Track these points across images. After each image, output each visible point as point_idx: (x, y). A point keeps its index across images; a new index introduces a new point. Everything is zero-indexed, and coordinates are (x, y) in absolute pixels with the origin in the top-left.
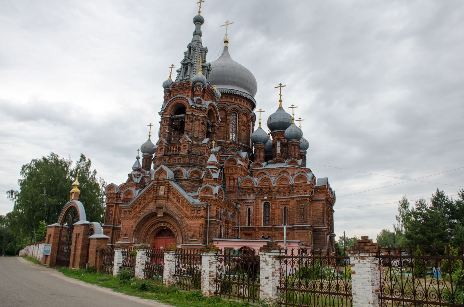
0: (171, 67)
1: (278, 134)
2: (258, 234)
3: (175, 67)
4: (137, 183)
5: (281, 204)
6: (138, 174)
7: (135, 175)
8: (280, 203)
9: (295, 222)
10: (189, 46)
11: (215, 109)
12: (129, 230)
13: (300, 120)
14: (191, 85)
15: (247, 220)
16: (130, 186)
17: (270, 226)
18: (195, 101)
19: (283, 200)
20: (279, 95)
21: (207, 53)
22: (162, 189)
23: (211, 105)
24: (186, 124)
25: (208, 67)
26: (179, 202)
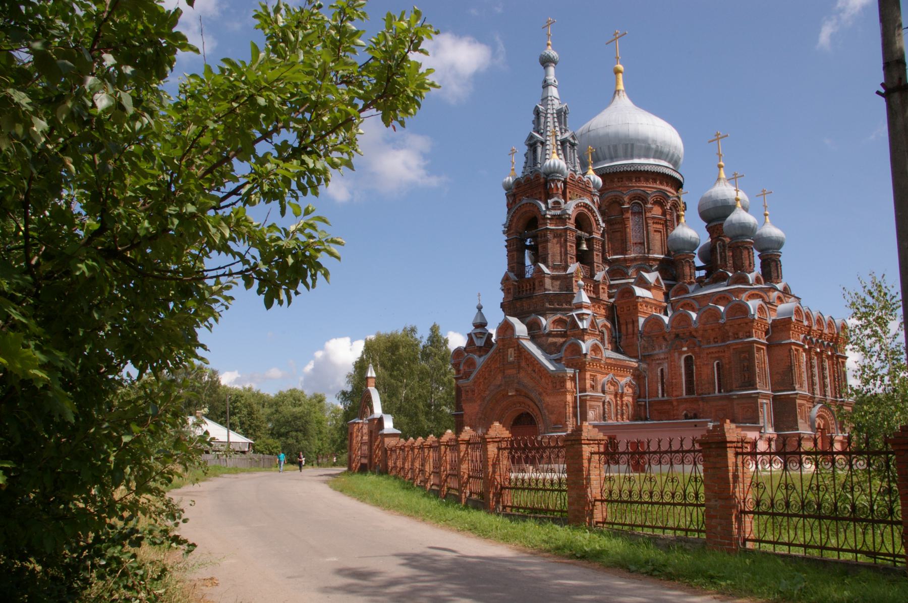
2: (677, 410)
5: (711, 358)
8: (710, 356)
9: (734, 386)
11: (591, 211)
12: (473, 417)
13: (764, 194)
14: (542, 180)
16: (471, 352)
17: (695, 396)
18: (550, 207)
19: (714, 350)
23: (581, 206)
24: (539, 246)
26: (534, 371)
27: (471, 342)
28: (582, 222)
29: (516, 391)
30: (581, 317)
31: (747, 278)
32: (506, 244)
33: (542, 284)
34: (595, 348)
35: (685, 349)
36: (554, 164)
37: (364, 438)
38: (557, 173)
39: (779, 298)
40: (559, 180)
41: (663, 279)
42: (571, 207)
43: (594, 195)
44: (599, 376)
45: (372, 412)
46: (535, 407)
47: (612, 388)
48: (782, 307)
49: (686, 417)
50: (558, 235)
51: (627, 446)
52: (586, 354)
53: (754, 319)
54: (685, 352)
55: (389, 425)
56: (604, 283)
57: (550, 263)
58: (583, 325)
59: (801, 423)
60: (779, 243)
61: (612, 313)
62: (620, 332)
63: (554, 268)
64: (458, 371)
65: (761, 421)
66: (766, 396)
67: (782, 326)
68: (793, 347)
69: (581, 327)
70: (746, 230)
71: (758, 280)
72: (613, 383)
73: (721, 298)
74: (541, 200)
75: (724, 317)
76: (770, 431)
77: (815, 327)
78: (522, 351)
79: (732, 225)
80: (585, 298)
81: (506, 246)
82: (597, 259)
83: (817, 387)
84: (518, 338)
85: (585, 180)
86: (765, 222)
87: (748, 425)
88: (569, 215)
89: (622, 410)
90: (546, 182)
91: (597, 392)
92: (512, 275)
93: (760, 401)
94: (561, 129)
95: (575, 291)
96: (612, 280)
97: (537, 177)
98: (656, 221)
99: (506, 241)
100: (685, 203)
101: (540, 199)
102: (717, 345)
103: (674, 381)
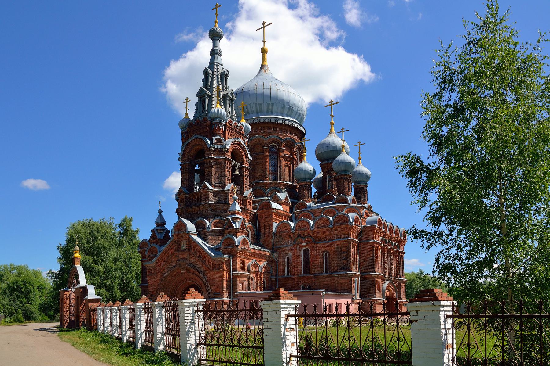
0: (186, 101)
1: (328, 167)
3: (190, 101)
4: (161, 239)
6: (161, 229)
7: (159, 230)
9: (336, 269)
10: (205, 71)
11: (243, 148)
14: (208, 123)
15: (286, 270)
16: (154, 243)
18: (214, 142)
20: (330, 115)
21: (229, 78)
22: (184, 244)
23: (236, 144)
24: (206, 170)
25: (230, 95)
27: (153, 235)
28: (235, 155)
29: (187, 270)
30: (235, 220)
31: (347, 199)
32: (181, 167)
33: (207, 197)
34: (244, 242)
35: (304, 244)
36: (218, 111)
37: (72, 302)
38: (220, 118)
39: (366, 213)
40: (221, 124)
41: (290, 199)
42: (229, 143)
43: (246, 137)
44: (246, 261)
45: (78, 283)
46: (200, 281)
47: (254, 269)
48: (369, 219)
49: (303, 289)
50: (217, 163)
51: (245, 305)
52: (238, 246)
53: (352, 225)
54: (304, 246)
55: (92, 292)
56: (250, 199)
57: (213, 182)
58: (236, 226)
59: (377, 293)
60: (367, 177)
61: (254, 220)
62: (260, 232)
63: (215, 186)
64: (143, 257)
65: (353, 291)
66: (356, 276)
67: (369, 230)
68: (375, 245)
69: (235, 227)
70: (348, 166)
71: (353, 202)
72: (256, 266)
73: (330, 211)
74: (207, 138)
75: (332, 224)
76: (358, 299)
77: (388, 233)
78: (191, 243)
79: (339, 162)
80: (238, 207)
81: (181, 169)
82: (246, 182)
83: (387, 271)
84: (189, 233)
85: (239, 125)
86: (359, 163)
87: (346, 294)
88: (228, 149)
89: (261, 284)
90: (211, 124)
91: (244, 271)
92: (184, 190)
93: (353, 279)
94: (223, 87)
95: (230, 203)
96: (256, 197)
97: (205, 120)
98: (286, 159)
99: (181, 165)
100: (306, 148)
101: (207, 137)
102: (326, 242)
103: (296, 265)
